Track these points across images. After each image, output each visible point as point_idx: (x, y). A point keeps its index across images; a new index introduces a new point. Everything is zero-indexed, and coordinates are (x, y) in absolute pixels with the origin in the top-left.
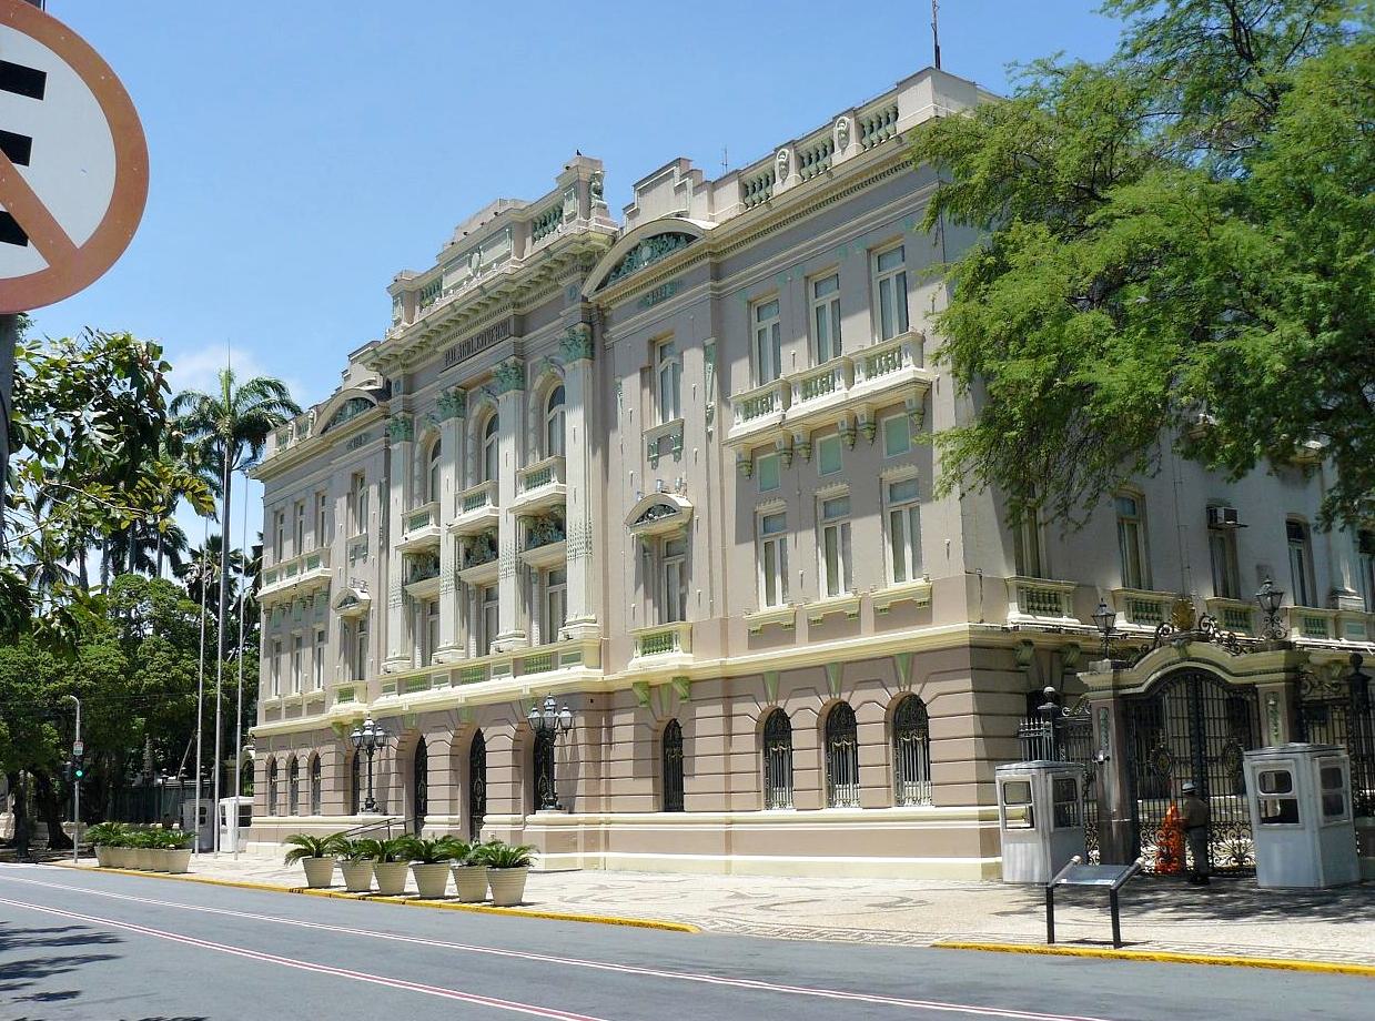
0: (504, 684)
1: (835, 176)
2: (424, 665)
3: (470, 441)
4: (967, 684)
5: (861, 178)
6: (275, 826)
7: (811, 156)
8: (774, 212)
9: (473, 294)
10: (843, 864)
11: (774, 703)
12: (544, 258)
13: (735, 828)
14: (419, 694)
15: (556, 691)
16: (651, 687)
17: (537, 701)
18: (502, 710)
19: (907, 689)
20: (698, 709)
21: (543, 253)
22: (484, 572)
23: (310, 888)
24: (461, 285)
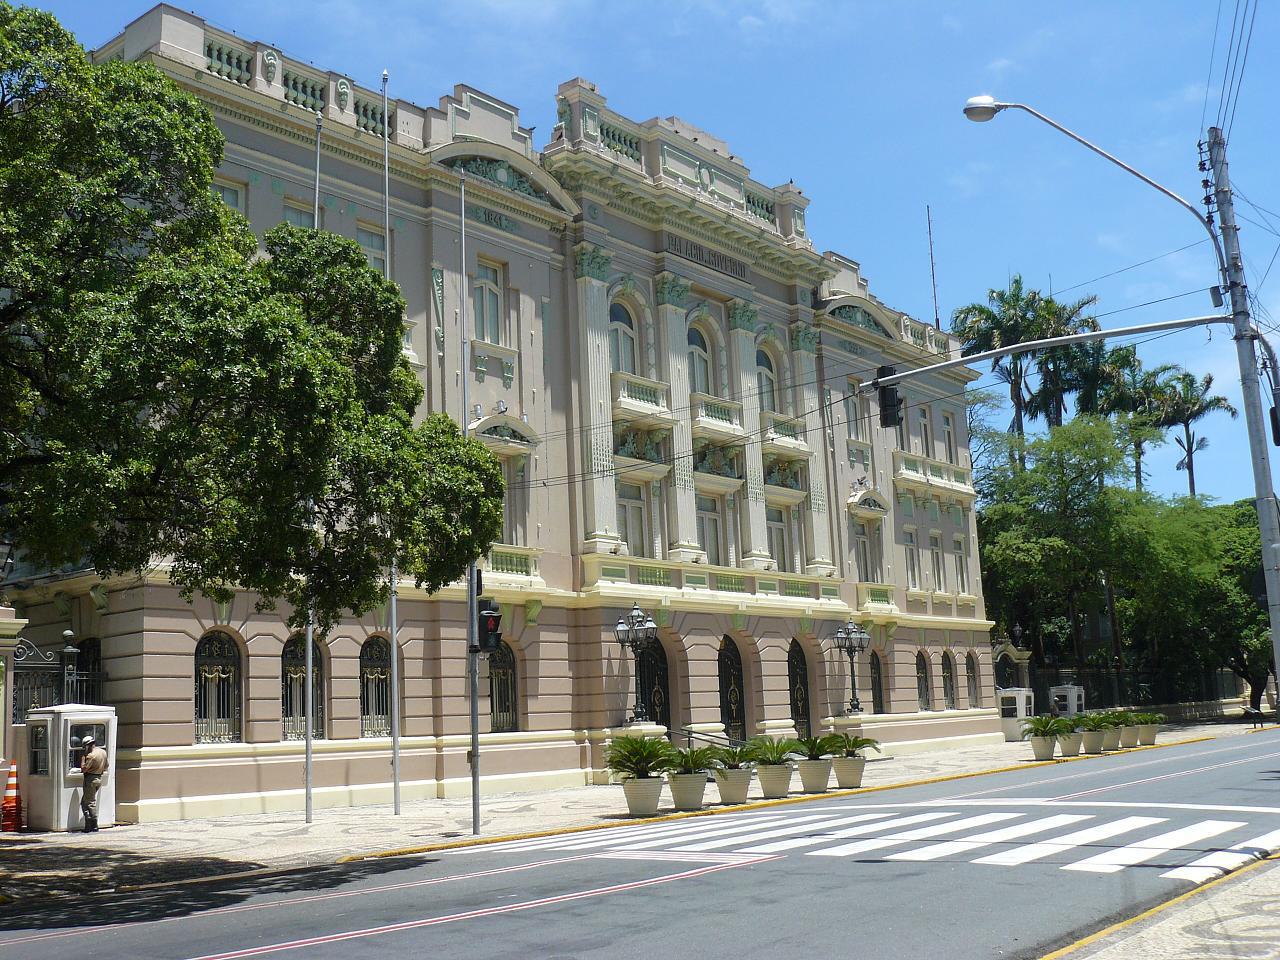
0: (769, 600)
1: (202, 80)
2: (664, 558)
3: (725, 363)
4: (565, 637)
5: (333, 142)
6: (250, 761)
7: (310, 89)
8: (355, 143)
9: (752, 229)
10: (945, 742)
11: (225, 623)
12: (816, 261)
13: (262, 760)
14: (734, 594)
15: (646, 605)
16: (112, 591)
17: (654, 612)
18: (770, 624)
19: (384, 629)
20: (895, 646)
21: (758, 231)
22: (782, 495)
23: (840, 788)
24: (677, 178)
